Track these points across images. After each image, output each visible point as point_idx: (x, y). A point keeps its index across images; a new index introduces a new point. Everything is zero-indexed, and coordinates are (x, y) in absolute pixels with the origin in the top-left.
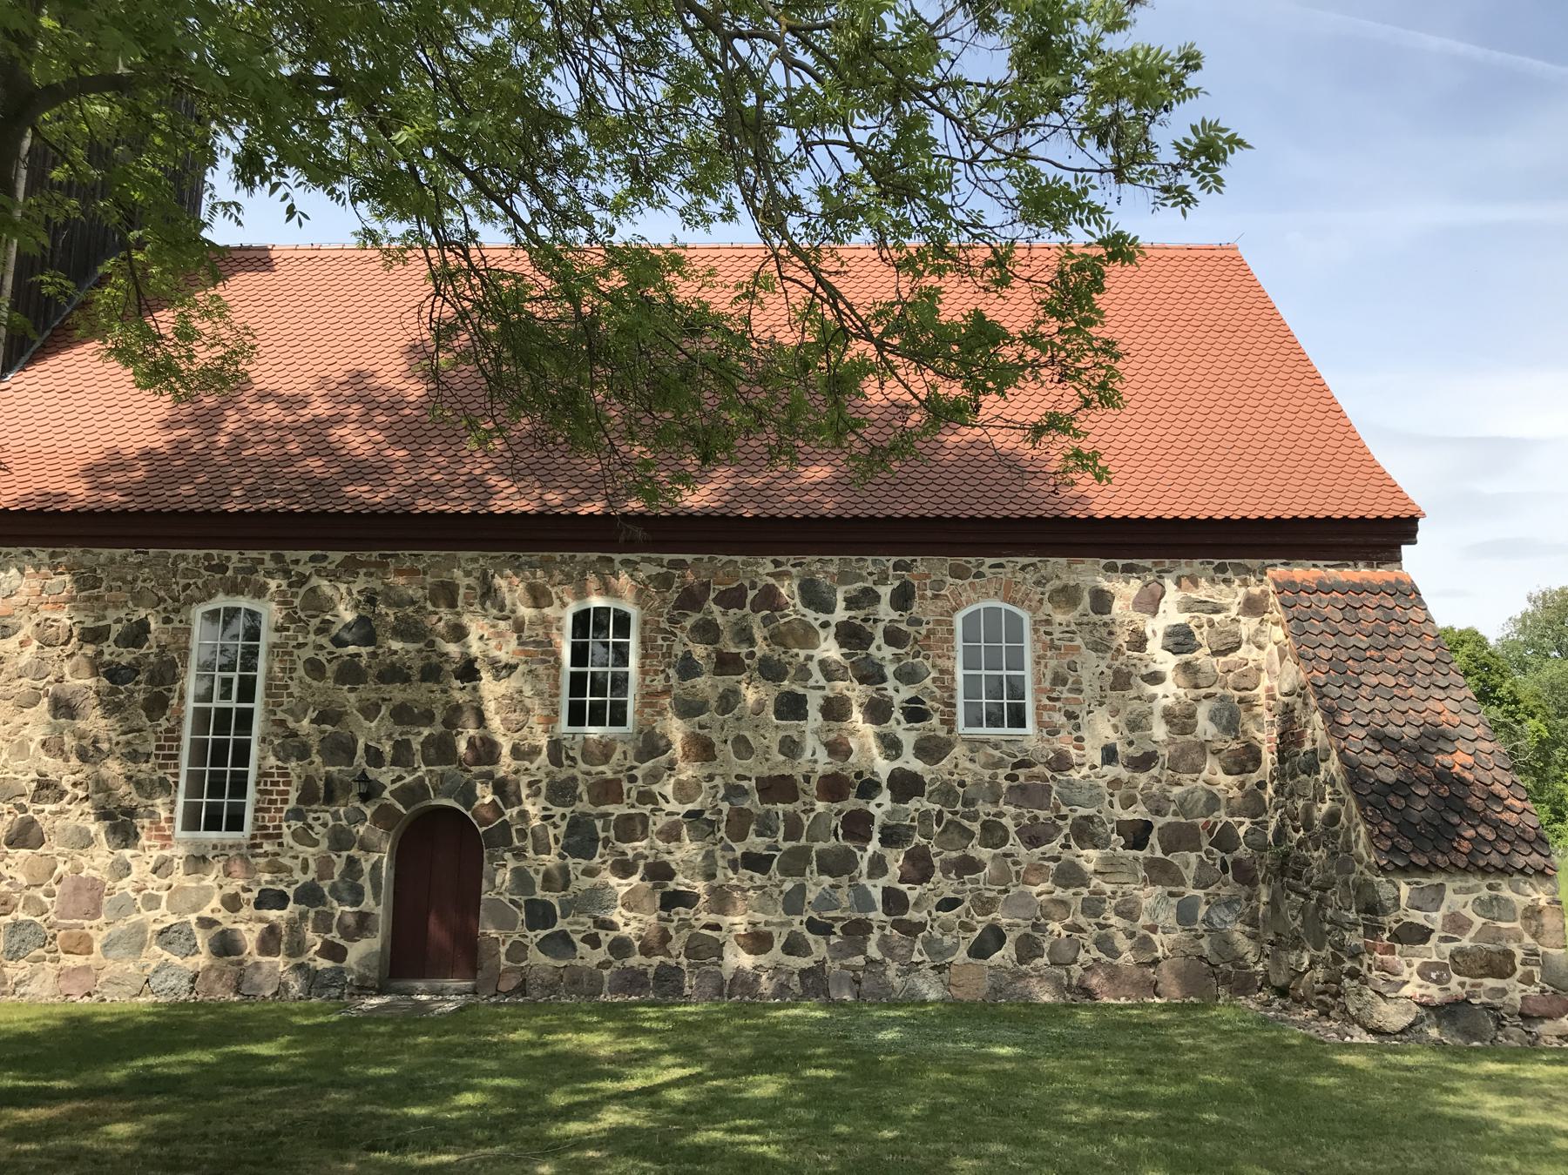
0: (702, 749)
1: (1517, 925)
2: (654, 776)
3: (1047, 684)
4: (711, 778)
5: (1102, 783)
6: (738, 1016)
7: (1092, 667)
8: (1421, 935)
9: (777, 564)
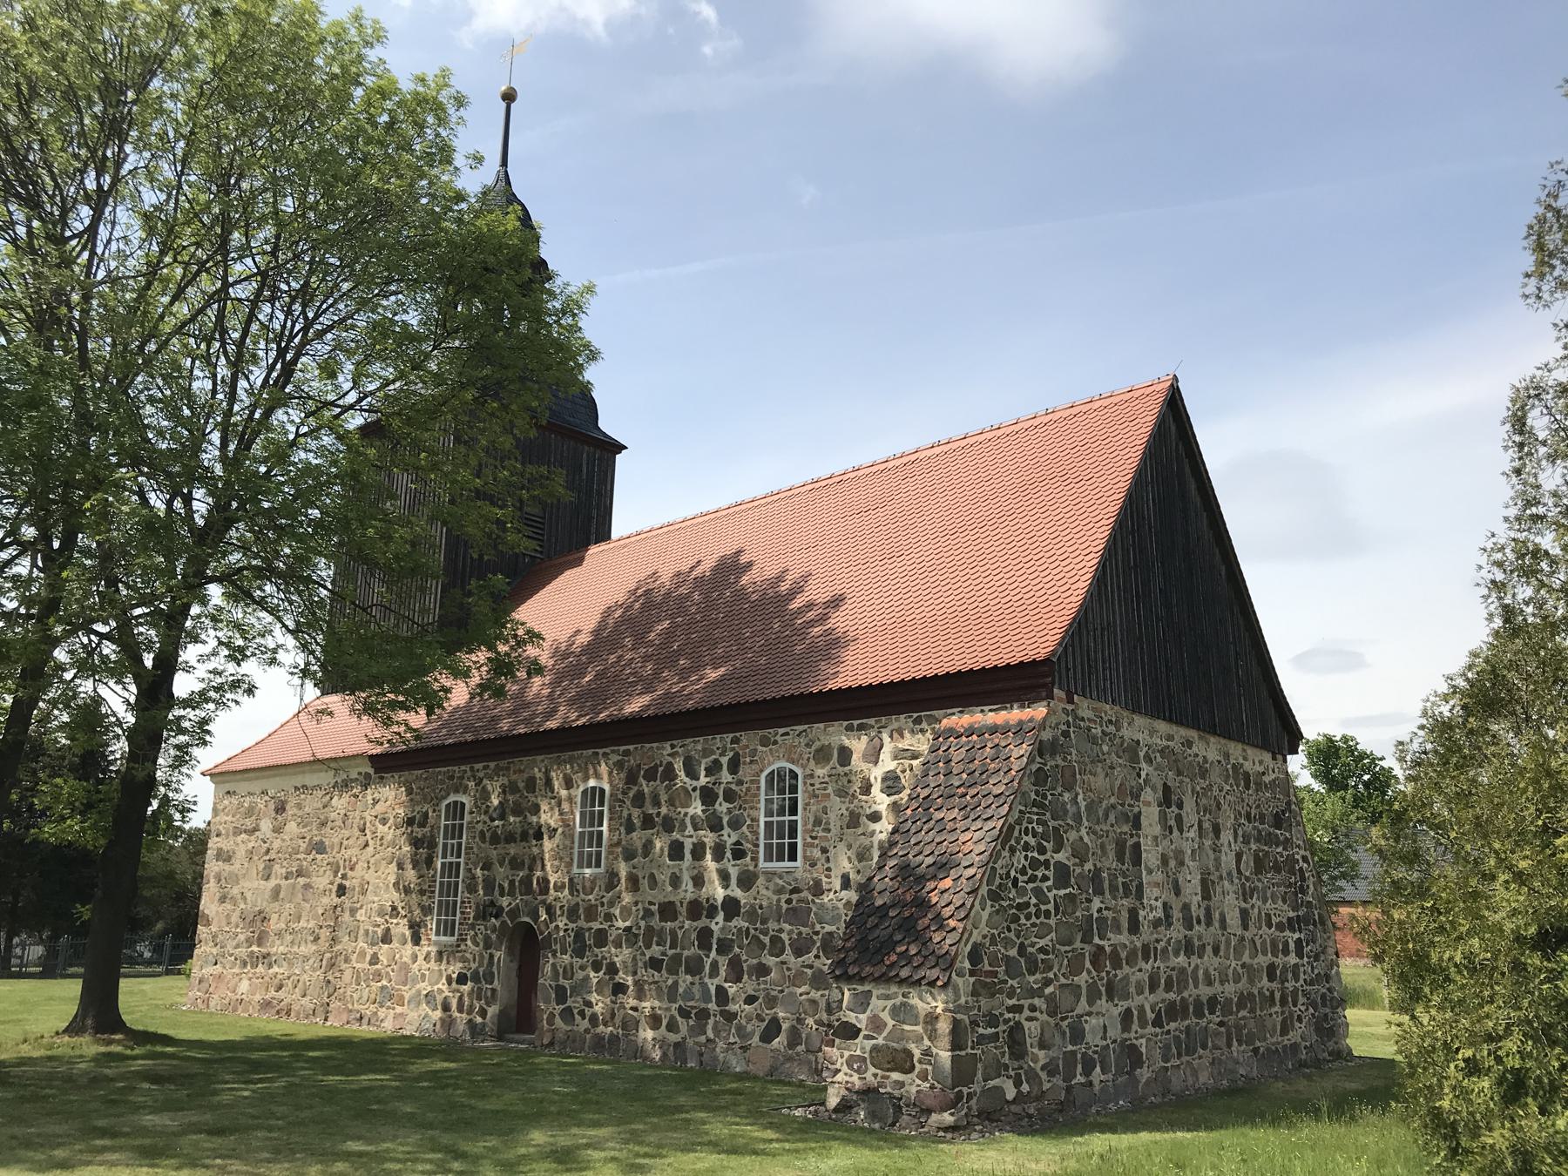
0: (634, 882)
1: (919, 1028)
2: (611, 904)
3: (810, 827)
4: (636, 903)
5: (840, 905)
6: (897, 1104)
7: (837, 809)
8: (850, 1032)
9: (673, 746)
